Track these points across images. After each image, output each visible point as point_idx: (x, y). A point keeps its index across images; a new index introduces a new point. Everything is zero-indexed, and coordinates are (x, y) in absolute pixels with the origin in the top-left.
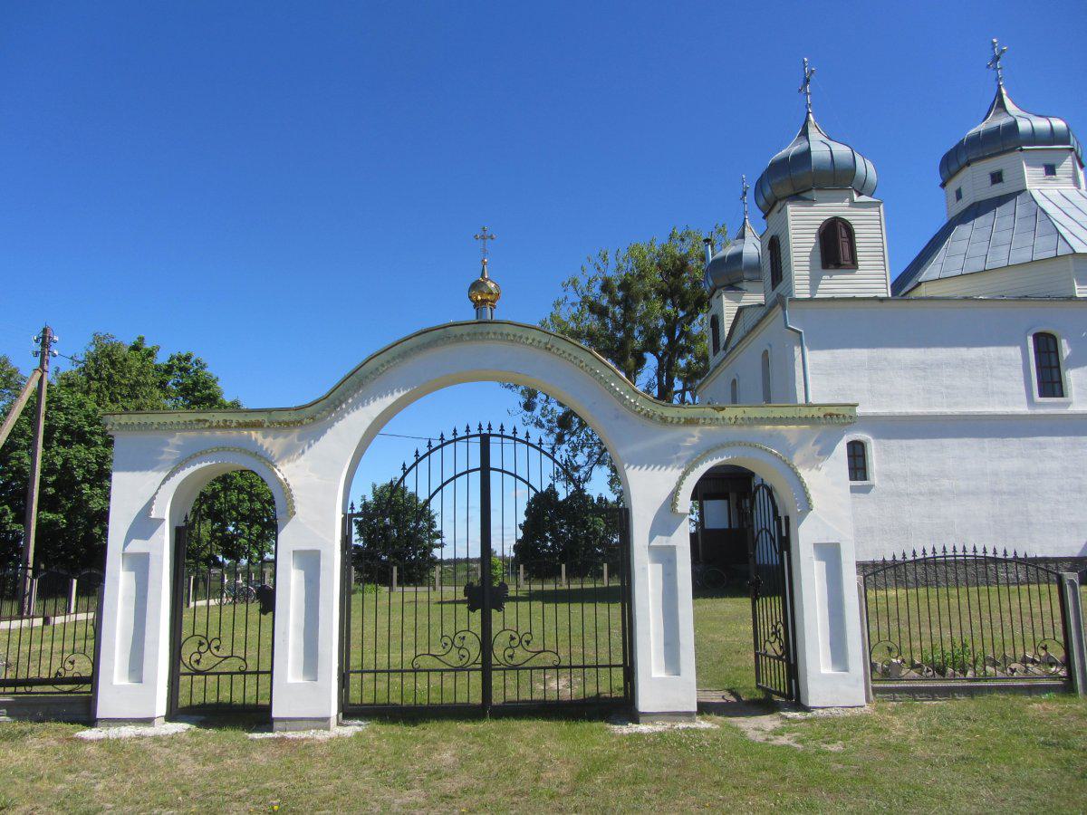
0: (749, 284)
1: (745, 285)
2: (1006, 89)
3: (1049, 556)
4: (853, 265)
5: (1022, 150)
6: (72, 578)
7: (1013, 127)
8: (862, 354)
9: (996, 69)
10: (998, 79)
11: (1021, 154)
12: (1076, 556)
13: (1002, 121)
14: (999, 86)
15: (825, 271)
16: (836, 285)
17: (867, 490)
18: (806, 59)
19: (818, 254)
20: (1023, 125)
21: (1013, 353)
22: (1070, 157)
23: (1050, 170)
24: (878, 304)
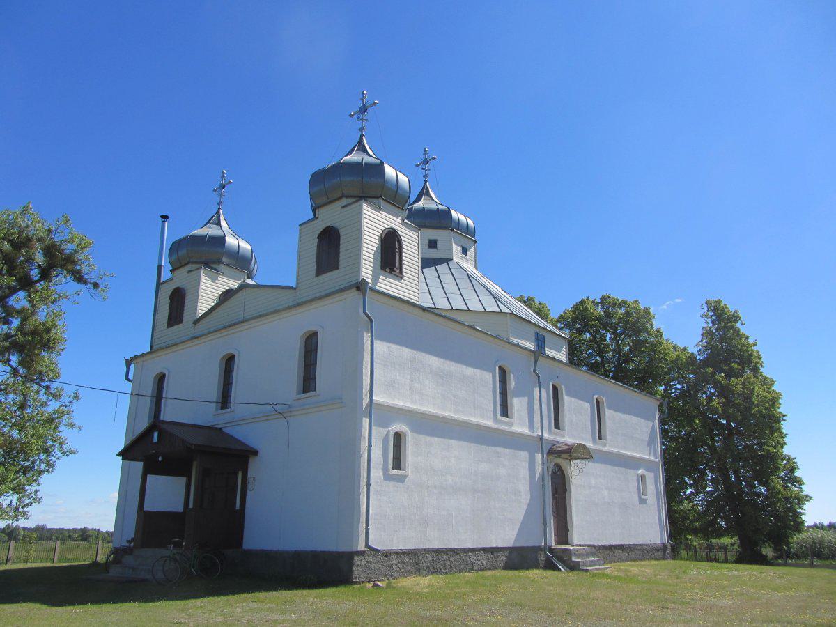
0: (226, 267)
1: (222, 268)
2: (433, 191)
3: (499, 546)
4: (400, 276)
5: (452, 230)
6: (191, 509)
7: (221, 240)
8: (407, 353)
9: (220, 195)
10: (220, 203)
11: (452, 233)
12: (511, 546)
13: (219, 233)
14: (219, 209)
15: (383, 272)
16: (387, 284)
17: (402, 479)
18: (365, 92)
19: (379, 255)
20: (231, 241)
21: (488, 377)
22: (202, 274)
23: (465, 251)
24: (421, 312)
